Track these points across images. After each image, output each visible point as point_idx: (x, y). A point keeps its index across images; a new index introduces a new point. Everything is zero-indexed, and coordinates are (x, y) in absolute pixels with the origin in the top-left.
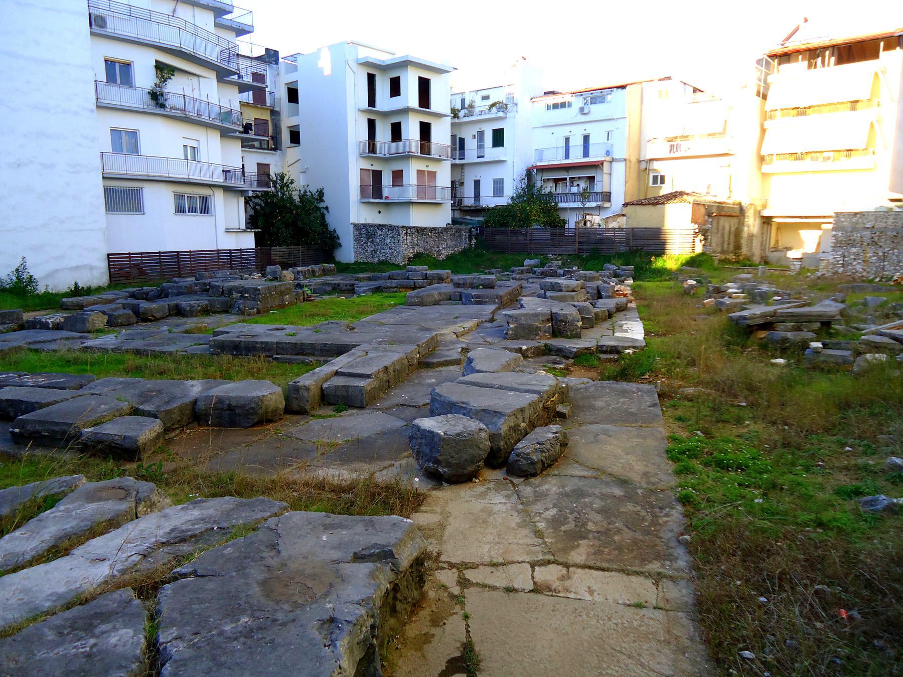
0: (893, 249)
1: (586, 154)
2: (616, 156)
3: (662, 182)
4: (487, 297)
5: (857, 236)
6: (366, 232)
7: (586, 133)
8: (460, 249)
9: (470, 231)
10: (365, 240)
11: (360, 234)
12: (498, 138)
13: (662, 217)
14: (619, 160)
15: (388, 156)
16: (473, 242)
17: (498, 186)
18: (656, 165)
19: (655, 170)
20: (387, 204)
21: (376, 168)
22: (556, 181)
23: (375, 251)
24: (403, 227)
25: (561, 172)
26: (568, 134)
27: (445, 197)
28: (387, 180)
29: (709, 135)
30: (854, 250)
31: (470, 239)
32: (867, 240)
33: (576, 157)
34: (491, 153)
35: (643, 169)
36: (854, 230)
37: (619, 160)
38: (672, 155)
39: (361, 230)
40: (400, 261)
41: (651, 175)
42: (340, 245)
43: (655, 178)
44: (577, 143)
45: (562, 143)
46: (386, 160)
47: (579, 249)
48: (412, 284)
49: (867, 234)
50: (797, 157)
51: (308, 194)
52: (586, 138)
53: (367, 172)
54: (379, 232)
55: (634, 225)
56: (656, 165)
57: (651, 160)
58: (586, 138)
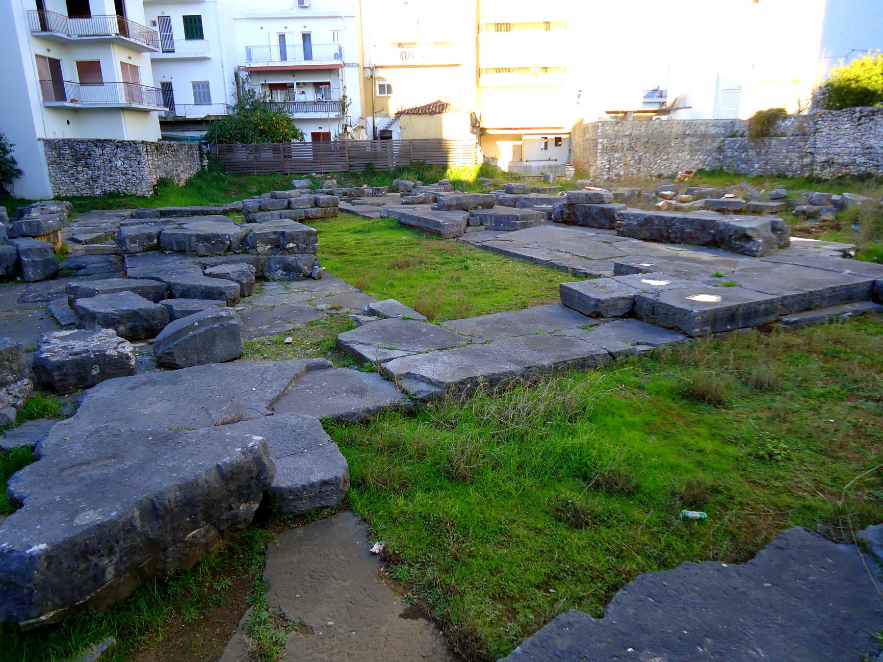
0: (646, 153)
1: (308, 55)
2: (347, 59)
3: (390, 91)
4: (532, 216)
5: (618, 142)
6: (69, 154)
7: (306, 31)
8: (194, 172)
9: (200, 149)
10: (70, 163)
11: (60, 155)
12: (194, 28)
13: (440, 127)
14: (352, 65)
15: (75, 38)
16: (206, 162)
17: (202, 92)
18: (380, 73)
19: (381, 79)
20: (75, 110)
21: (53, 55)
22: (273, 87)
23: (95, 179)
24: (143, 142)
25: (281, 79)
26: (282, 30)
27: (152, 102)
28: (70, 73)
29: (436, 43)
30: (617, 155)
31: (201, 158)
32: (626, 146)
33: (295, 58)
34: (184, 47)
35: (370, 76)
36: (617, 137)
37: (352, 65)
38: (405, 63)
39: (61, 148)
40: (146, 190)
41: (378, 83)
42: (19, 173)
43: (382, 87)
44: (294, 42)
45: (275, 41)
46: (65, 44)
47: (350, 166)
48: (303, 214)
49: (626, 140)
50: (498, 70)
51: (824, 50)
52: (306, 37)
53: (42, 61)
54: (99, 151)
55: (411, 136)
56: (380, 73)
57: (377, 67)
58: (306, 37)
